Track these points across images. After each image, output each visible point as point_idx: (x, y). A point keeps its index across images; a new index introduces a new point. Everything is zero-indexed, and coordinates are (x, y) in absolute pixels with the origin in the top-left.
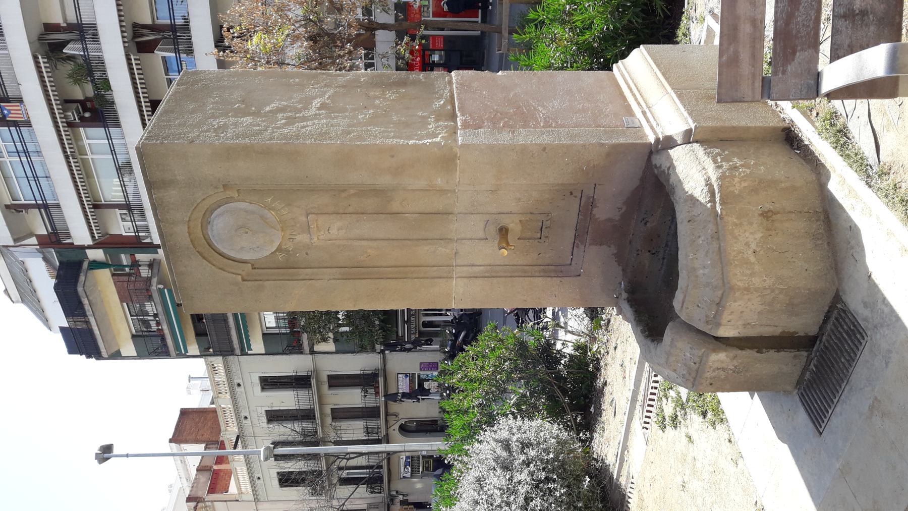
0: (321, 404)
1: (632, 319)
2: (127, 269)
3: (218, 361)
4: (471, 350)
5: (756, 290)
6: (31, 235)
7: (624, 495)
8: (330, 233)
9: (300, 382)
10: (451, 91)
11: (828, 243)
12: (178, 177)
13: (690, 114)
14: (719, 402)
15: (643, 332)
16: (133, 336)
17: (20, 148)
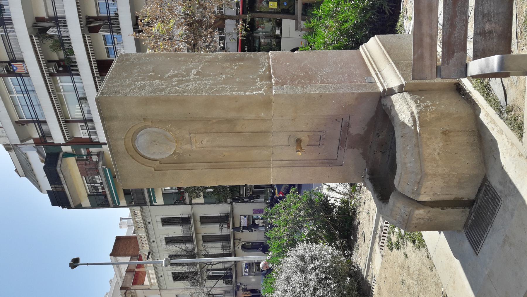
0: (196, 233)
1: (372, 189)
2: (85, 157)
3: (137, 209)
4: (282, 204)
5: (440, 175)
6: (30, 138)
7: (370, 287)
8: (203, 143)
9: (184, 221)
10: (269, 63)
11: (480, 148)
12: (119, 115)
13: (402, 76)
14: (422, 236)
15: (378, 197)
16: (89, 195)
17: (23, 89)
